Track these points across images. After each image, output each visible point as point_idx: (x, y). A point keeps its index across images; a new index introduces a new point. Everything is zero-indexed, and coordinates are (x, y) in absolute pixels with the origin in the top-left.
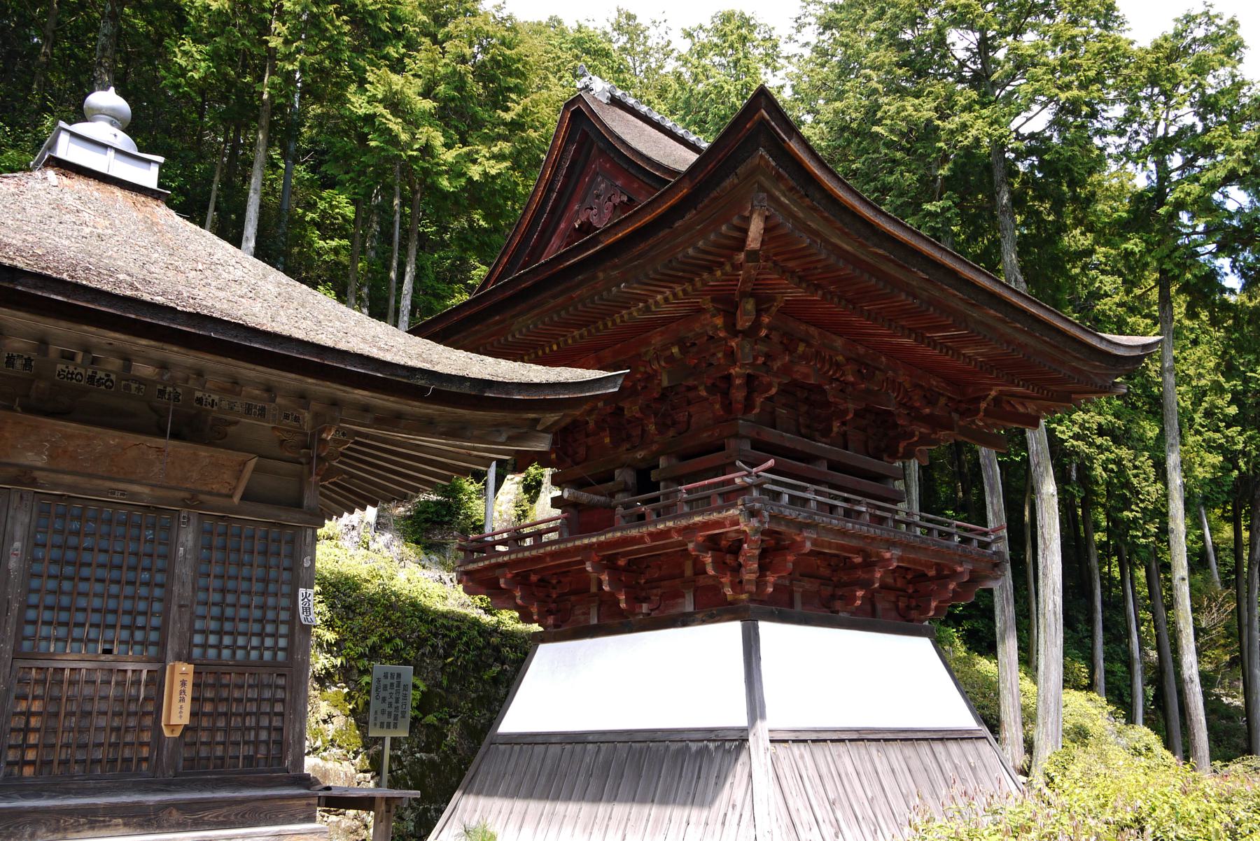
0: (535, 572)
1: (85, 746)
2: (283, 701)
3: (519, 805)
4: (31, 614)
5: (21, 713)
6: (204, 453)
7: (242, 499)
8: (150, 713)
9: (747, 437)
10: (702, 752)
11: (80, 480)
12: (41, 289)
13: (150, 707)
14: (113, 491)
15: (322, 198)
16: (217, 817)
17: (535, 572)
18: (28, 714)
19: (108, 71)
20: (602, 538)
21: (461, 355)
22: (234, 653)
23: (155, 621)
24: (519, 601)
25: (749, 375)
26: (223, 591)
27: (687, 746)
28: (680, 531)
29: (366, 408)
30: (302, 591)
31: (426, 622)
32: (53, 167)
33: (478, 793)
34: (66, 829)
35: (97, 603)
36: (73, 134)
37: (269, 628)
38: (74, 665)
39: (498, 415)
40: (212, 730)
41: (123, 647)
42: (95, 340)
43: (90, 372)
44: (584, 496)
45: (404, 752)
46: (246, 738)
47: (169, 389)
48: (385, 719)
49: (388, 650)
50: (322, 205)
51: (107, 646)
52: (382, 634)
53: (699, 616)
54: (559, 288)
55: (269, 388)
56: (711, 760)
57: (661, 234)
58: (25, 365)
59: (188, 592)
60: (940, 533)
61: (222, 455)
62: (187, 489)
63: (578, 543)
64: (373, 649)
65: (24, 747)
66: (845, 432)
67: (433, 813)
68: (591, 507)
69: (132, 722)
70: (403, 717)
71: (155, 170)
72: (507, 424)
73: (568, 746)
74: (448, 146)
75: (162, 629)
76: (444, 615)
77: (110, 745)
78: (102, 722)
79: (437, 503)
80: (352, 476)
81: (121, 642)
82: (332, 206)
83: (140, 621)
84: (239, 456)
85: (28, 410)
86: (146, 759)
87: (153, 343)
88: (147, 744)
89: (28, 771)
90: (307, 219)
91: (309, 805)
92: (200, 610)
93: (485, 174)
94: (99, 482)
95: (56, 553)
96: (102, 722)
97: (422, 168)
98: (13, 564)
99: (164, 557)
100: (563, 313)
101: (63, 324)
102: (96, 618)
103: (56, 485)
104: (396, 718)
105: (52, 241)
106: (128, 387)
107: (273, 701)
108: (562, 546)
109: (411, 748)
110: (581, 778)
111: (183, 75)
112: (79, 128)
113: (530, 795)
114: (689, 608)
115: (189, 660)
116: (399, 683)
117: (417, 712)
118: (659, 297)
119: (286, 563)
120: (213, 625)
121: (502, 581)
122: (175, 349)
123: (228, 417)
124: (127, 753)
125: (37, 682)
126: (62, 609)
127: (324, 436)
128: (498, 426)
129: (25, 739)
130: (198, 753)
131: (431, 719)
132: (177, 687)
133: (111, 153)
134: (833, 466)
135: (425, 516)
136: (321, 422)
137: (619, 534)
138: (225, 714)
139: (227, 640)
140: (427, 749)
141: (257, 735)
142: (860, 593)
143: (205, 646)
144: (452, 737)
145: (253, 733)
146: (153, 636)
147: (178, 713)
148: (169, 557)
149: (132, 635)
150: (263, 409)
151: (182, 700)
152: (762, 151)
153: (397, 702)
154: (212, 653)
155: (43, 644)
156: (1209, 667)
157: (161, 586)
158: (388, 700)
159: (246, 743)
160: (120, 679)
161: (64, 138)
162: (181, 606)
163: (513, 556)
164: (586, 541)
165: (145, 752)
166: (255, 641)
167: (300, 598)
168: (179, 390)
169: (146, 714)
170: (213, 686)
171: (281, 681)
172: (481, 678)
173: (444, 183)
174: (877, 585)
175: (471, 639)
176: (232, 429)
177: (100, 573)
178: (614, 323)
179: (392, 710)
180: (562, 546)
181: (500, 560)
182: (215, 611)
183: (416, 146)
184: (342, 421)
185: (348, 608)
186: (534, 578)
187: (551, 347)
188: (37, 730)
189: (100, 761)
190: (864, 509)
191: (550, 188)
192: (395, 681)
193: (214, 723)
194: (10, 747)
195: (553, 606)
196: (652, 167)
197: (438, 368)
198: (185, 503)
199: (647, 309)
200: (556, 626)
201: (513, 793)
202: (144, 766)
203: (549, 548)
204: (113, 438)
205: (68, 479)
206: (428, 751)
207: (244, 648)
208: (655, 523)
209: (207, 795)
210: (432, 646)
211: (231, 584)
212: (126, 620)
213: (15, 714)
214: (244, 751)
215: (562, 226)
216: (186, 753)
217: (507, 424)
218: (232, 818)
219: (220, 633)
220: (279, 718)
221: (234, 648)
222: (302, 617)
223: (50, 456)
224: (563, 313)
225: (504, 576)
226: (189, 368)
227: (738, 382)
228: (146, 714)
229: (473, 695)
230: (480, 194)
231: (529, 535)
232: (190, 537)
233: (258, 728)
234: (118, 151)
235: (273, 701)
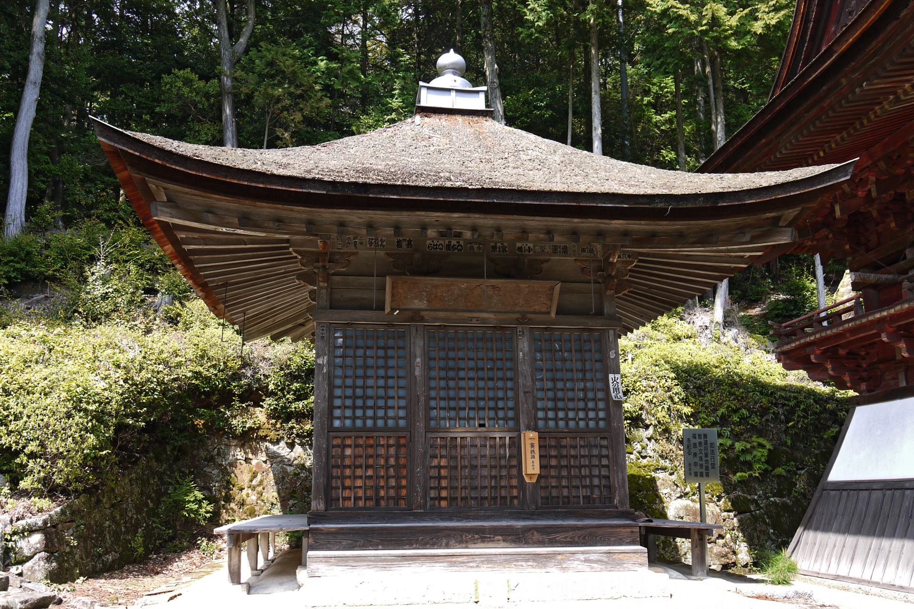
0: (842, 346)
1: (476, 488)
2: (607, 456)
3: (850, 540)
4: (433, 403)
5: (435, 467)
6: (524, 285)
7: (557, 314)
8: (515, 466)
11: (449, 314)
12: (383, 193)
13: (514, 462)
14: (471, 319)
15: (654, 84)
16: (565, 538)
17: (842, 346)
18: (439, 467)
19: (490, 40)
20: (892, 311)
22: (567, 424)
23: (511, 404)
24: (831, 372)
26: (554, 380)
29: (625, 233)
30: (611, 376)
31: (767, 395)
33: (816, 529)
34: (467, 542)
35: (472, 394)
36: (429, 88)
37: (591, 405)
38: (462, 435)
39: (739, 220)
40: (559, 478)
41: (492, 422)
42: (427, 220)
44: (872, 277)
45: (759, 496)
46: (584, 483)
47: (499, 245)
48: (698, 469)
49: (736, 418)
50: (655, 89)
51: (482, 422)
52: (728, 407)
54: (809, 102)
55: (549, 232)
57: (889, 28)
58: (408, 245)
59: (529, 383)
61: (536, 284)
62: (518, 312)
63: (871, 318)
64: (723, 417)
65: (439, 488)
69: (504, 472)
70: (713, 468)
71: (482, 96)
72: (751, 226)
73: (888, 492)
74: (732, 14)
75: (515, 409)
76: (783, 389)
77: (492, 487)
78: (485, 472)
79: (784, 301)
80: (651, 287)
81: (490, 419)
82: (661, 88)
83: (501, 404)
84: (547, 284)
85: (414, 273)
86: (516, 497)
87: (462, 215)
88: (515, 487)
89: (444, 504)
90: (645, 102)
91: (632, 532)
92: (540, 394)
93: (767, 26)
94: (461, 314)
95: (442, 364)
96: (485, 472)
97: (712, 38)
98: (417, 372)
99: (511, 360)
100: (817, 123)
101: (405, 213)
102: (472, 404)
103: (436, 319)
104: (707, 468)
106: (472, 248)
107: (600, 457)
108: (858, 322)
109: (765, 494)
110: (902, 520)
111: (533, 26)
112: (435, 83)
113: (858, 532)
115: (535, 429)
116: (706, 442)
117: (766, 466)
118: (907, 85)
119: (597, 356)
120: (550, 404)
121: (812, 357)
122: (477, 216)
123: (542, 258)
124: (503, 493)
125: (441, 447)
126: (450, 399)
127: (611, 259)
128: (741, 229)
129: (439, 483)
130: (550, 493)
131: (779, 471)
133: (453, 93)
135: (776, 312)
136: (609, 250)
137: (906, 306)
138: (566, 466)
139: (370, 413)
140: (779, 494)
141: (591, 481)
143: (546, 419)
144: (800, 485)
145: (588, 480)
146: (511, 414)
147: (532, 466)
148: (514, 359)
149: (496, 414)
151: (533, 457)
153: (706, 455)
154: (551, 424)
155: (442, 422)
157: (511, 379)
158: (698, 455)
159: (583, 487)
160: (492, 443)
161: (424, 92)
162: (525, 393)
163: (818, 336)
164: (878, 316)
165: (515, 493)
166: (581, 415)
167: (611, 381)
168: (505, 244)
169: (512, 467)
170: (555, 447)
171: (604, 443)
172: (822, 438)
173: (733, 44)
175: (809, 406)
176: (545, 265)
177: (472, 374)
178: (869, 120)
179: (703, 462)
180: (858, 322)
181: (808, 339)
182: (550, 394)
183: (704, 22)
184: (623, 246)
185: (699, 388)
186: (842, 352)
187: (818, 154)
188: (445, 478)
189: (486, 498)
191: (806, 20)
192: (702, 440)
193: (559, 473)
194: (431, 488)
195: (864, 374)
197: (674, 192)
198: (519, 322)
199: (898, 100)
200: (869, 391)
201: (845, 530)
202: (516, 502)
203: (846, 326)
204: (463, 284)
205: (442, 314)
206: (782, 496)
207: (574, 419)
209: (580, 523)
210: (774, 413)
211: (559, 375)
212: (491, 404)
213: (431, 467)
214: (583, 492)
216: (543, 494)
217: (751, 226)
218: (576, 539)
219: (556, 409)
220: (606, 469)
221: (567, 419)
222: (613, 395)
223: (428, 301)
224: (817, 123)
225: (814, 353)
226: (491, 227)
228: (512, 467)
229: (816, 452)
230: (769, 41)
231: (824, 319)
232: (526, 344)
233: (591, 476)
234: (458, 91)
235: (600, 457)
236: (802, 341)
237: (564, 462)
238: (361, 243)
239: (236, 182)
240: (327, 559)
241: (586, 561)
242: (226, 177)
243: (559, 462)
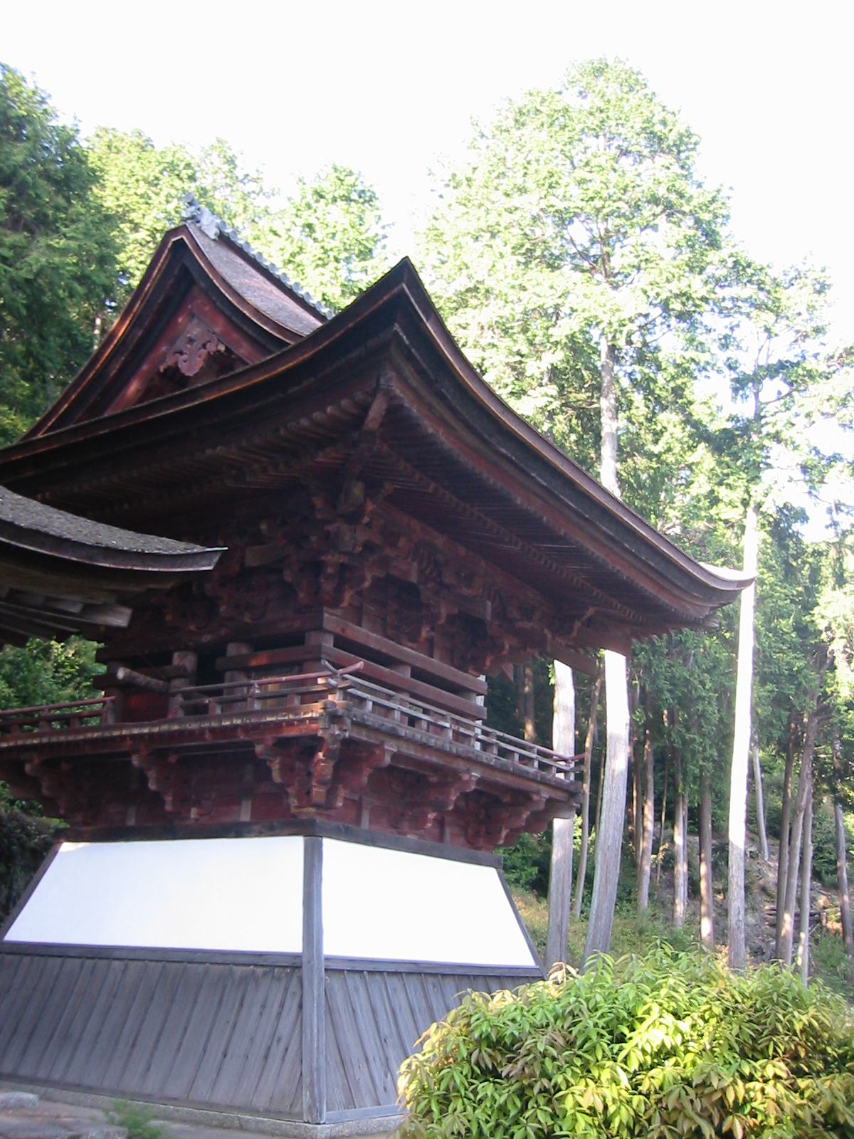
9: (330, 632)
10: (244, 980)
21: (102, 528)
25: (342, 565)
27: (231, 971)
28: (245, 728)
53: (256, 828)
56: (257, 985)
60: (522, 757)
63: (124, 732)
66: (432, 637)
68: (145, 690)
114: (245, 816)
121: (28, 767)
134: (418, 674)
142: (431, 816)
152: (397, 327)
174: (451, 808)
181: (29, 742)
190: (447, 725)
196: (259, 319)
208: (219, 718)
215: (145, 367)
227: (330, 570)
236: (20, 743)
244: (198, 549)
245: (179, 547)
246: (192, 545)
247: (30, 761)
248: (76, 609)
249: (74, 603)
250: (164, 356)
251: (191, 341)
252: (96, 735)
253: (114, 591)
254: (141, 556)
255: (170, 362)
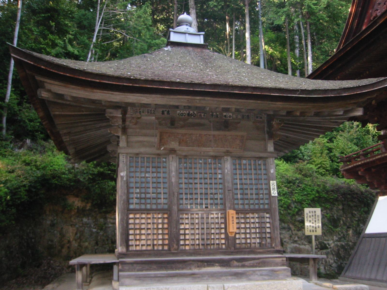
24: (368, 180)
32: (170, 45)
36: (174, 32)
43: (188, 112)
51: (206, 206)
59: (230, 185)
67: (344, 264)
71: (202, 37)
98: (173, 180)
105: (205, 79)
106: (200, 115)
108: (383, 156)
116: (315, 215)
121: (360, 173)
122: (209, 98)
132: (231, 219)
138: (249, 228)
150: (248, 116)
151: (233, 223)
156: (361, 225)
158: (312, 221)
161: (172, 34)
165: (223, 241)
167: (271, 184)
168: (218, 114)
170: (243, 218)
181: (358, 164)
192: (314, 214)
203: (377, 157)
236: (355, 165)
237: (248, 226)
238: (143, 112)
239: (84, 78)
240: (129, 277)
241: (261, 275)
242: (79, 76)
243: (245, 226)
244: (383, 78)
245: (373, 80)
246: (380, 78)
247: (360, 170)
248: (341, 113)
249: (340, 111)
250: (371, 13)
251: (379, 4)
252: (379, 157)
253: (354, 103)
254: (359, 88)
255: (374, 15)
